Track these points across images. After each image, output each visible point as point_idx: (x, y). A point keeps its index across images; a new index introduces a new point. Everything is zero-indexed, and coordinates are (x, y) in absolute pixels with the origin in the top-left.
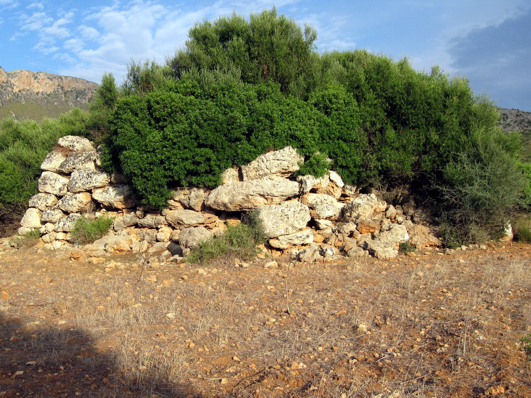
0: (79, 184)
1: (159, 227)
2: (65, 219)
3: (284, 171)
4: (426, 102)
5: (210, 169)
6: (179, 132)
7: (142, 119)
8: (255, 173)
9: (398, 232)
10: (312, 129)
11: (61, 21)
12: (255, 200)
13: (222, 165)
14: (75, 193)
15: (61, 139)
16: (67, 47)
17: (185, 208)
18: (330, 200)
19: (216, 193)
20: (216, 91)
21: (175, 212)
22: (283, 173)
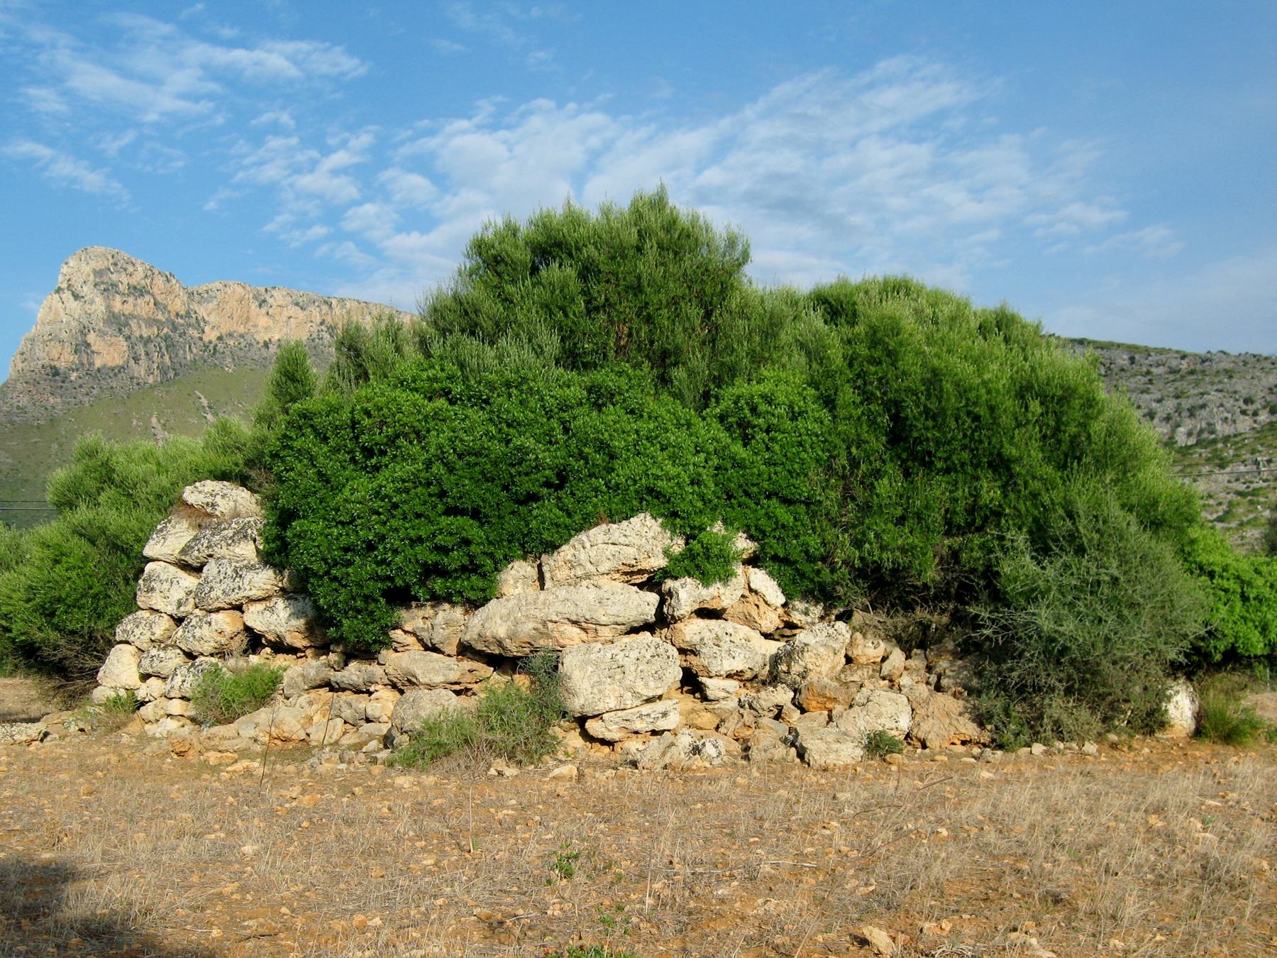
0: (217, 592)
1: (372, 689)
2: (184, 671)
3: (627, 569)
4: (969, 413)
5: (472, 562)
6: (404, 481)
7: (336, 450)
8: (567, 572)
9: (883, 709)
10: (699, 475)
11: (340, 158)
12: (562, 633)
13: (499, 555)
14: (210, 612)
15: (188, 489)
16: (350, 226)
17: (427, 648)
18: (742, 635)
19: (484, 615)
20: (493, 389)
21: (403, 658)
22: (626, 573)
